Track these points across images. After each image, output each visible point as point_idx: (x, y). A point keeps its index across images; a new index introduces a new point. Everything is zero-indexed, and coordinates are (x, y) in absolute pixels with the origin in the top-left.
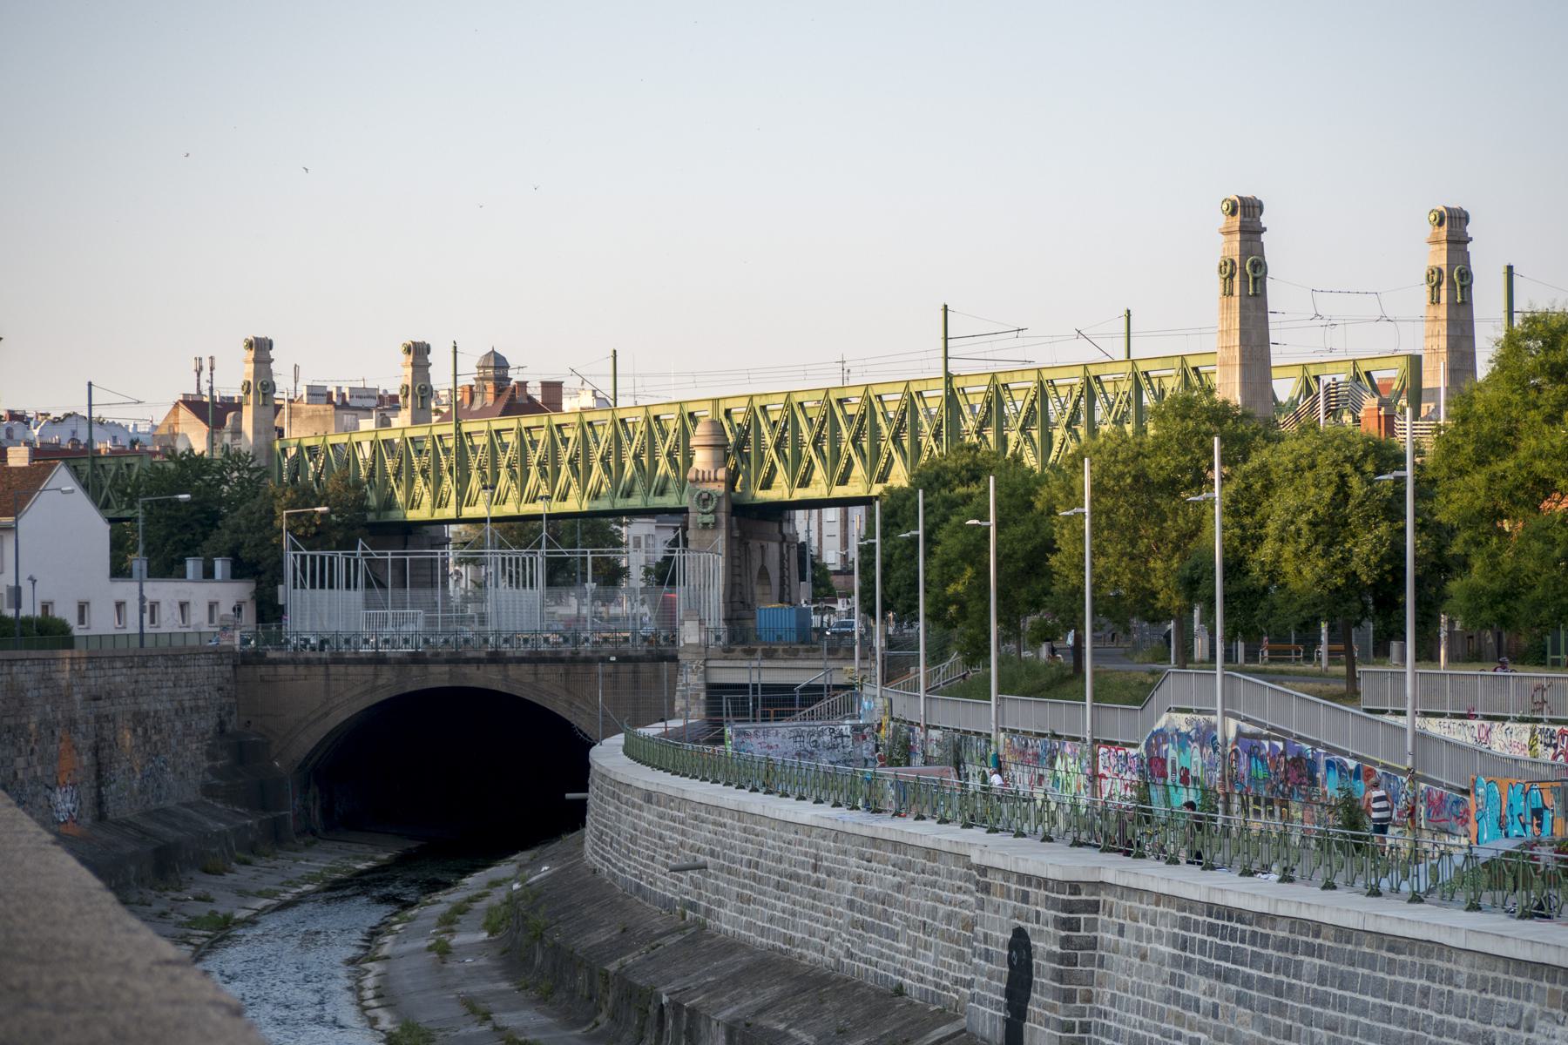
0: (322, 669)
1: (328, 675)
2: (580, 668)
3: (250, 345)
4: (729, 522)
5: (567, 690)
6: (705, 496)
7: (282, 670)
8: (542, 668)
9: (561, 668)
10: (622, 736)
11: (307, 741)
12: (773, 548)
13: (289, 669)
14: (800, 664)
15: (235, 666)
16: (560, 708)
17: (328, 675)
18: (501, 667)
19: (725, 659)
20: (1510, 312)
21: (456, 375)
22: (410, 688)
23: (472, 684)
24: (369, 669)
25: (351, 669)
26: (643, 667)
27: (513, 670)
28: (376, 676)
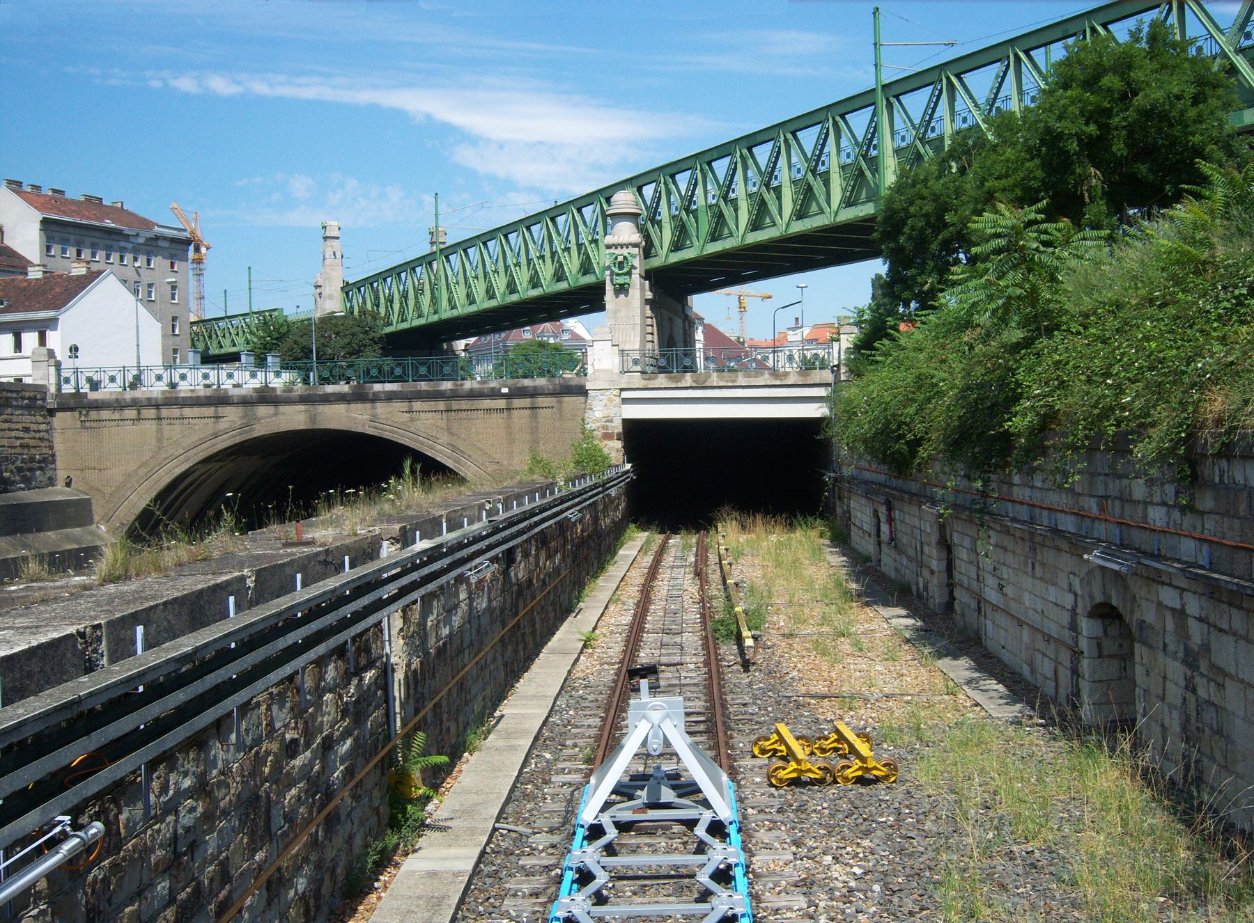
2: (464, 404)
4: (642, 286)
6: (620, 259)
8: (417, 405)
9: (441, 405)
11: (140, 498)
12: (678, 322)
18: (369, 405)
22: (260, 430)
24: (209, 411)
25: (187, 411)
27: (381, 408)
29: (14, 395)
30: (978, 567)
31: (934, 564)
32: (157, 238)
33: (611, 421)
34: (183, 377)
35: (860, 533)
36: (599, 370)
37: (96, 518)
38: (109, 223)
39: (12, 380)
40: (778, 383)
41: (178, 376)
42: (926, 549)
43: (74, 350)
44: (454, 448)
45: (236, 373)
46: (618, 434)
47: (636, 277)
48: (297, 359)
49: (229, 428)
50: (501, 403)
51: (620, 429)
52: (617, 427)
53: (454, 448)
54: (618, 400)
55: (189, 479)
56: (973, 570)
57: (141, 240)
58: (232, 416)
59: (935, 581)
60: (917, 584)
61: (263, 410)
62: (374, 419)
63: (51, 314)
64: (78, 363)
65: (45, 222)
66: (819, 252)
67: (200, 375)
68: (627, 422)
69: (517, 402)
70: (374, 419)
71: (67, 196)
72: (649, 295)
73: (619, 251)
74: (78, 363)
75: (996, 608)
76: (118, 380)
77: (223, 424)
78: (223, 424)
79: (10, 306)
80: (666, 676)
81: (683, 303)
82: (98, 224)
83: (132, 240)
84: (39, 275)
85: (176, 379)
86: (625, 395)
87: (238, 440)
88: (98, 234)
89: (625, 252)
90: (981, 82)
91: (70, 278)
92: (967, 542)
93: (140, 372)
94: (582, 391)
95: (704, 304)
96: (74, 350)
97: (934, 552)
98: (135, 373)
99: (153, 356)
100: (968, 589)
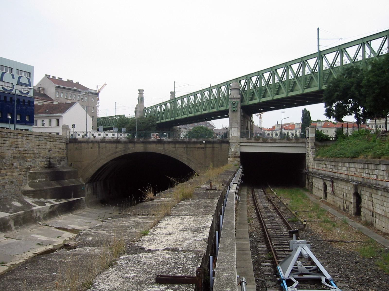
0: (97, 145)
1: (99, 147)
2: (192, 146)
3: (139, 90)
4: (240, 110)
5: (187, 153)
6: (234, 102)
7: (83, 145)
8: (177, 145)
9: (185, 146)
10: (228, 119)
11: (92, 171)
12: (249, 122)
13: (86, 145)
14: (277, 145)
15: (67, 144)
16: (185, 161)
17: (99, 147)
18: (162, 145)
19: (248, 142)
20: (262, 143)
21: (175, 88)
22: (129, 152)
23: (151, 151)
24: (114, 145)
25: (108, 145)
26: (215, 145)
27: (166, 145)
28: (116, 147)
29: (57, 139)
30: (373, 202)
31: (352, 200)
32: (89, 93)
33: (237, 152)
34: (107, 135)
35: (317, 189)
36: (233, 137)
37: (79, 176)
38: (75, 88)
39: (55, 134)
40: (289, 142)
41: (105, 134)
42: (348, 195)
43: (74, 126)
44: (188, 159)
45: (122, 134)
46: (239, 156)
47: (239, 109)
48: (131, 130)
49: (120, 151)
50: (203, 146)
51: (239, 155)
52: (239, 154)
53: (188, 159)
54: (239, 146)
55: (106, 166)
56: (370, 203)
57: (84, 93)
58: (121, 147)
59: (352, 206)
60: (344, 207)
61: (130, 145)
62: (164, 149)
63: (60, 114)
64: (75, 130)
65: (57, 87)
66: (296, 102)
67: (112, 134)
68: (242, 153)
69: (208, 145)
70: (164, 149)
71: (63, 80)
72: (242, 114)
73: (233, 100)
74: (75, 130)
75: (380, 215)
76: (101, 135)
77: (118, 149)
78: (118, 149)
79: (48, 112)
80: (301, 234)
81: (251, 116)
82: (72, 88)
83: (82, 93)
84: (57, 103)
85: (105, 136)
86: (242, 144)
87: (123, 154)
88: (72, 91)
89: (236, 100)
90: (352, 51)
91: (66, 104)
92: (368, 194)
93: (87, 133)
94: (228, 142)
95: (255, 117)
96: (74, 126)
97: (352, 197)
98: (85, 133)
99: (90, 129)
100: (368, 209)
